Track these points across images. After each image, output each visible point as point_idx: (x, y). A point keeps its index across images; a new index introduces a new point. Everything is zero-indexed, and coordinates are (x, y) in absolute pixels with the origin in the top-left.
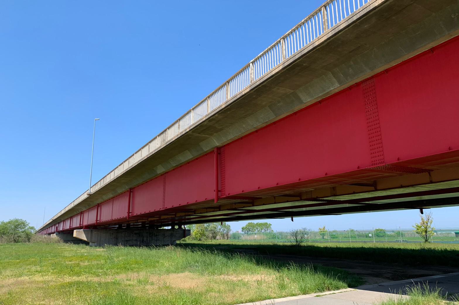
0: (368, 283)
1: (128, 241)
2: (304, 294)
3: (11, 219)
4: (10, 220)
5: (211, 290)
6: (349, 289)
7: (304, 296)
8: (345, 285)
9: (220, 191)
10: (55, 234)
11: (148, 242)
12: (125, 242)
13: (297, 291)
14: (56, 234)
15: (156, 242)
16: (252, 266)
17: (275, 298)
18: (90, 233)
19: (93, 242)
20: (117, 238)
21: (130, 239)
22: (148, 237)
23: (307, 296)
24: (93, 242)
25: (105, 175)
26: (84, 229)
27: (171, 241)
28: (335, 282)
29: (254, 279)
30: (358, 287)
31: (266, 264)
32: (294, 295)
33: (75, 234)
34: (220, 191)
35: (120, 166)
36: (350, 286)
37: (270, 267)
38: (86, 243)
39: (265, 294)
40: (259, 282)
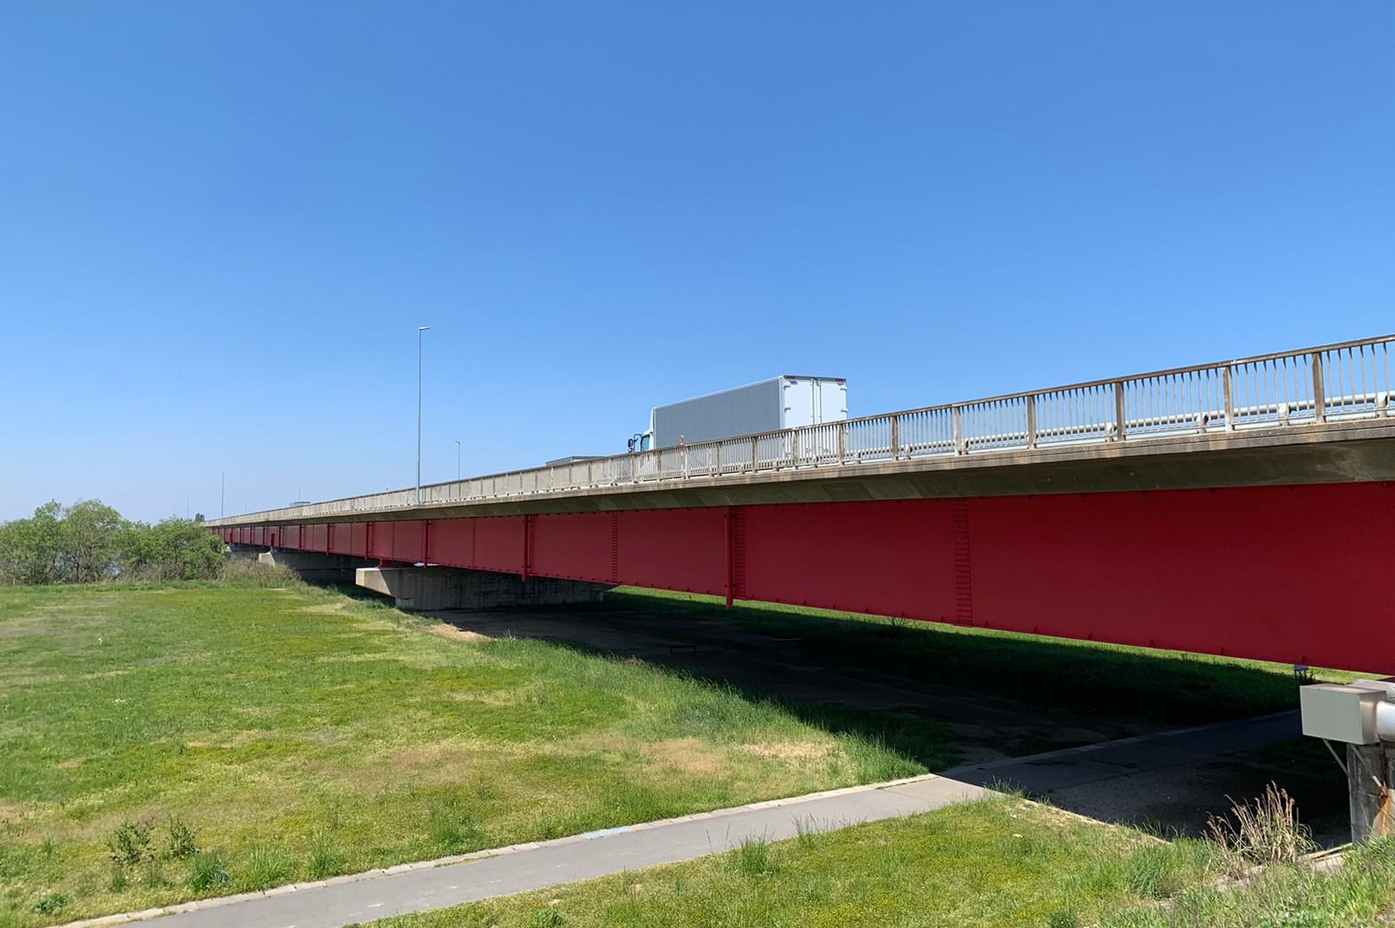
0: (965, 763)
1: (487, 593)
2: (863, 784)
3: (163, 518)
4: (161, 520)
5: (735, 778)
6: (931, 776)
7: (862, 787)
8: (925, 769)
9: (735, 586)
10: (269, 553)
11: (536, 595)
12: (482, 598)
13: (852, 779)
14: (273, 554)
15: (553, 594)
16: (792, 723)
17: (822, 791)
18: (397, 575)
19: (405, 597)
20: (461, 589)
21: (492, 589)
22: (536, 583)
23: (867, 788)
24: (405, 599)
25: (467, 478)
26: (383, 566)
27: (591, 591)
28: (909, 764)
29: (795, 753)
30: (946, 773)
31: (815, 722)
32: (847, 786)
33: (362, 577)
34: (735, 586)
35: (511, 477)
36: (932, 771)
37: (821, 727)
38: (388, 600)
39: (808, 786)
40: (803, 761)
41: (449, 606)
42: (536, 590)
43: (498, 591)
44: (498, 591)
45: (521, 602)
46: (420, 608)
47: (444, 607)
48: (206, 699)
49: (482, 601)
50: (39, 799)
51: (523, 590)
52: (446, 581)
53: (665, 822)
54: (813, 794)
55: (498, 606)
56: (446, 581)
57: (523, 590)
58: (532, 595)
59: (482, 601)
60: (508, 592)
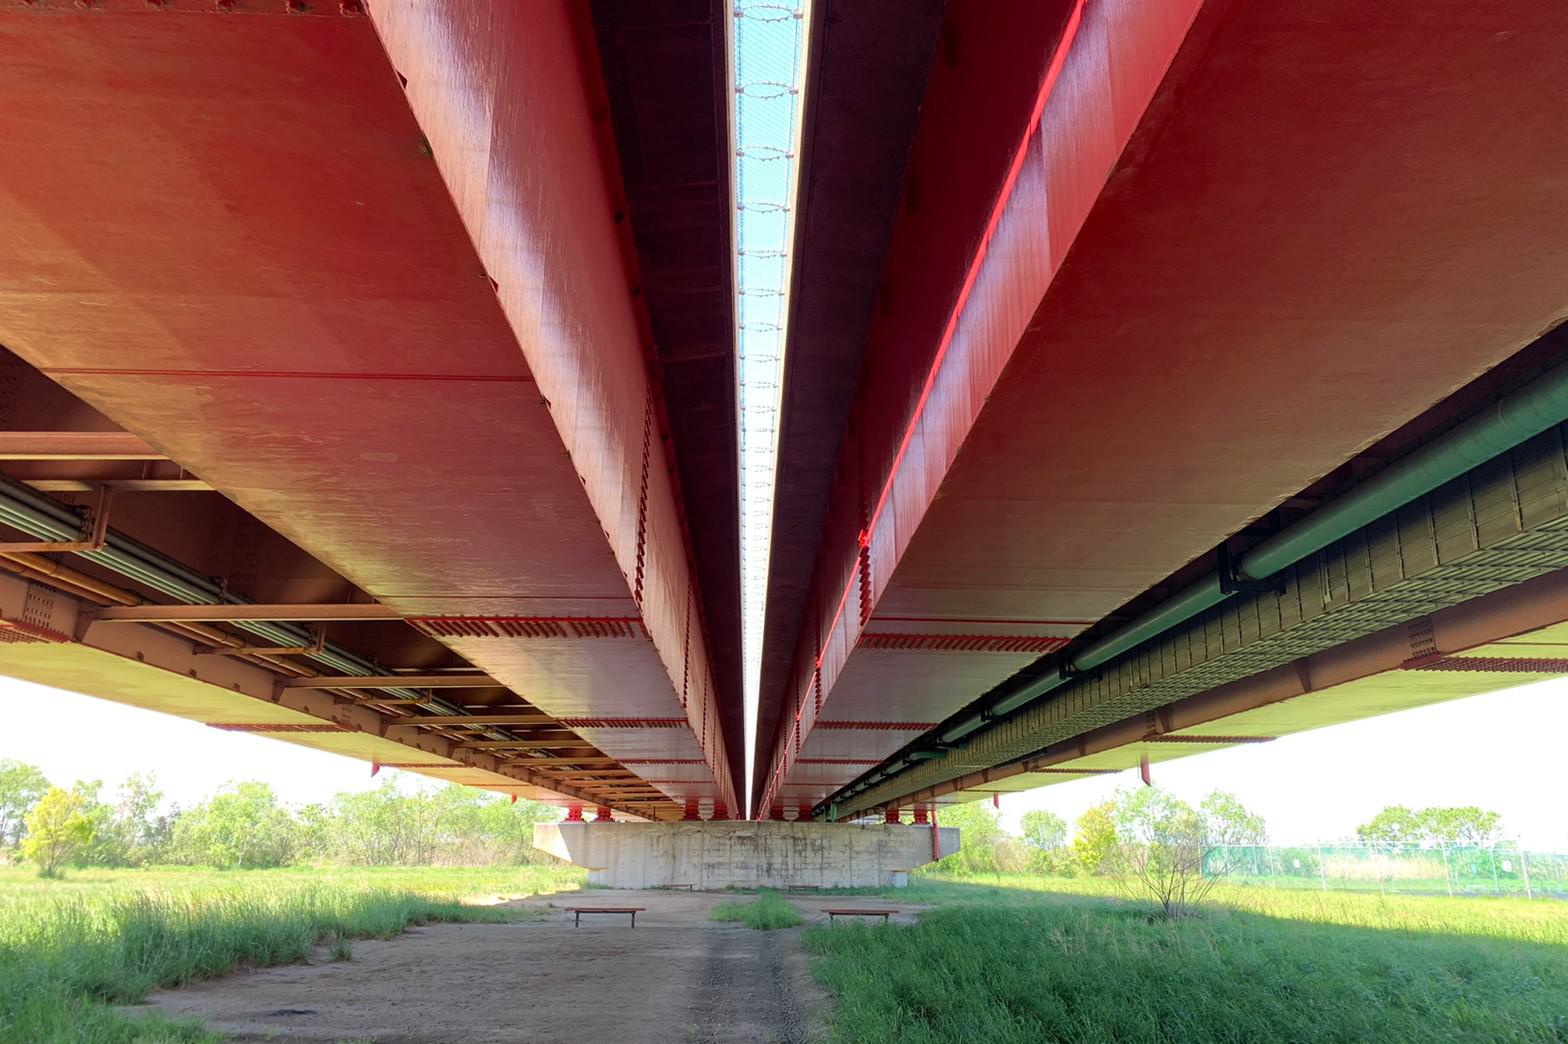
1: (713, 866)
11: (791, 872)
20: (674, 857)
21: (721, 860)
22: (790, 854)
41: (655, 884)
42: (790, 866)
43: (730, 864)
44: (730, 864)
45: (765, 881)
46: (668, 882)
47: (648, 885)
48: (1180, 928)
49: (705, 878)
50: (1466, 983)
51: (770, 864)
52: (652, 845)
53: (1155, 89)
54: (1179, 45)
55: (664, 886)
56: (652, 845)
57: (770, 864)
58: (784, 873)
59: (705, 878)
60: (745, 866)
